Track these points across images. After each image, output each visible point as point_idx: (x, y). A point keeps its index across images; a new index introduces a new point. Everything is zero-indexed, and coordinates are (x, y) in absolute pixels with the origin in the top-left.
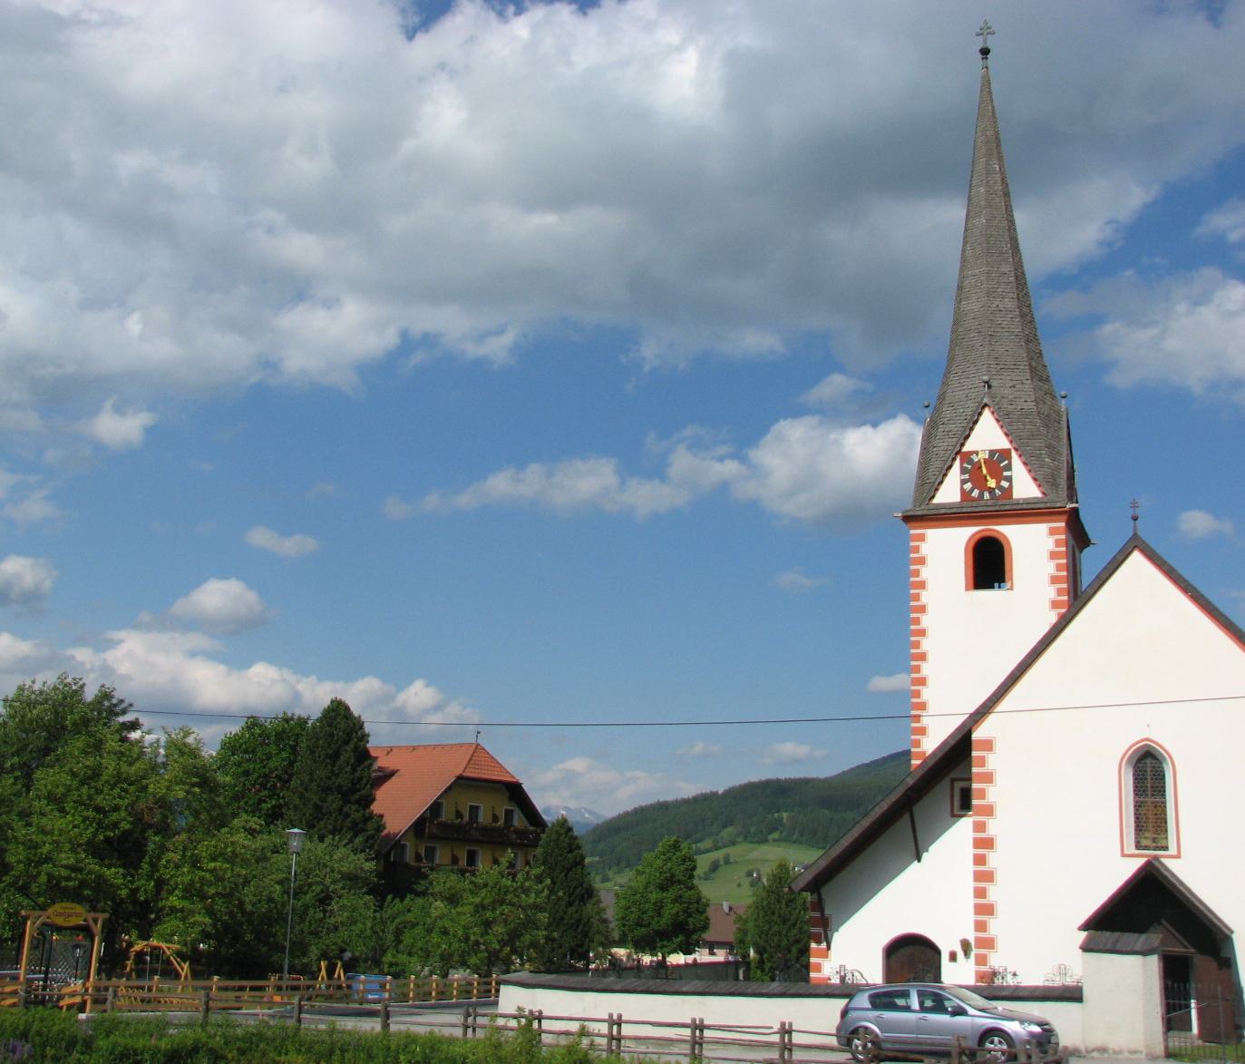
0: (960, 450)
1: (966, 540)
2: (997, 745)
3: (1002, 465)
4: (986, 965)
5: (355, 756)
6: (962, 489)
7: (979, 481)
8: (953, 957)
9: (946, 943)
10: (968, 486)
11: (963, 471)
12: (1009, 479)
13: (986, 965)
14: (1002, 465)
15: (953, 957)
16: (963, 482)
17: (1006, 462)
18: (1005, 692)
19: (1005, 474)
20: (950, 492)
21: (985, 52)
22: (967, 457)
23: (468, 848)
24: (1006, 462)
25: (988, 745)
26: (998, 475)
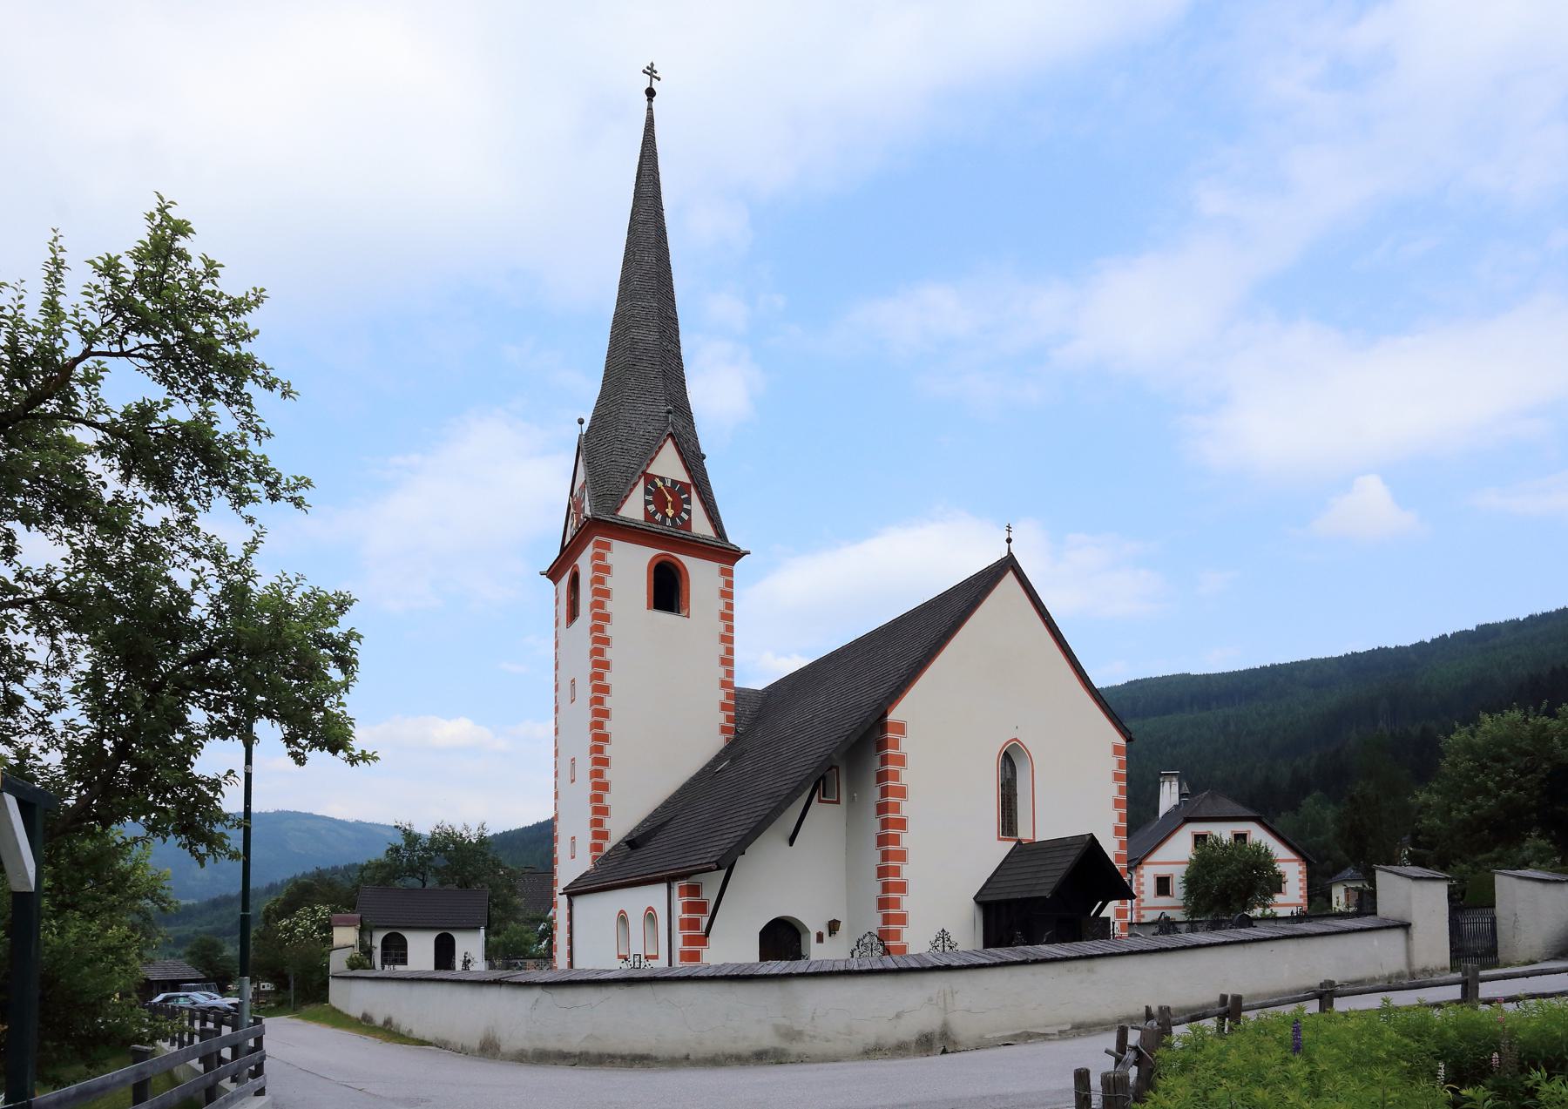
0: (646, 470)
1: (649, 560)
2: (909, 729)
3: (682, 497)
4: (699, 930)
5: (93, 494)
6: (646, 509)
7: (661, 504)
8: (820, 938)
9: (813, 923)
10: (652, 508)
11: (647, 492)
12: (688, 512)
13: (699, 930)
14: (682, 497)
15: (820, 938)
16: (647, 503)
17: (686, 496)
18: (1071, 662)
19: (685, 506)
20: (634, 508)
21: (650, 93)
22: (650, 479)
23: (1474, 740)
24: (686, 496)
25: (900, 728)
26: (678, 508)
